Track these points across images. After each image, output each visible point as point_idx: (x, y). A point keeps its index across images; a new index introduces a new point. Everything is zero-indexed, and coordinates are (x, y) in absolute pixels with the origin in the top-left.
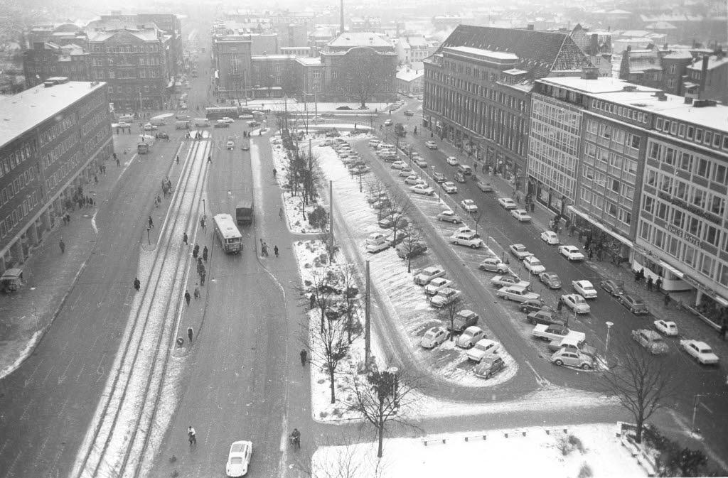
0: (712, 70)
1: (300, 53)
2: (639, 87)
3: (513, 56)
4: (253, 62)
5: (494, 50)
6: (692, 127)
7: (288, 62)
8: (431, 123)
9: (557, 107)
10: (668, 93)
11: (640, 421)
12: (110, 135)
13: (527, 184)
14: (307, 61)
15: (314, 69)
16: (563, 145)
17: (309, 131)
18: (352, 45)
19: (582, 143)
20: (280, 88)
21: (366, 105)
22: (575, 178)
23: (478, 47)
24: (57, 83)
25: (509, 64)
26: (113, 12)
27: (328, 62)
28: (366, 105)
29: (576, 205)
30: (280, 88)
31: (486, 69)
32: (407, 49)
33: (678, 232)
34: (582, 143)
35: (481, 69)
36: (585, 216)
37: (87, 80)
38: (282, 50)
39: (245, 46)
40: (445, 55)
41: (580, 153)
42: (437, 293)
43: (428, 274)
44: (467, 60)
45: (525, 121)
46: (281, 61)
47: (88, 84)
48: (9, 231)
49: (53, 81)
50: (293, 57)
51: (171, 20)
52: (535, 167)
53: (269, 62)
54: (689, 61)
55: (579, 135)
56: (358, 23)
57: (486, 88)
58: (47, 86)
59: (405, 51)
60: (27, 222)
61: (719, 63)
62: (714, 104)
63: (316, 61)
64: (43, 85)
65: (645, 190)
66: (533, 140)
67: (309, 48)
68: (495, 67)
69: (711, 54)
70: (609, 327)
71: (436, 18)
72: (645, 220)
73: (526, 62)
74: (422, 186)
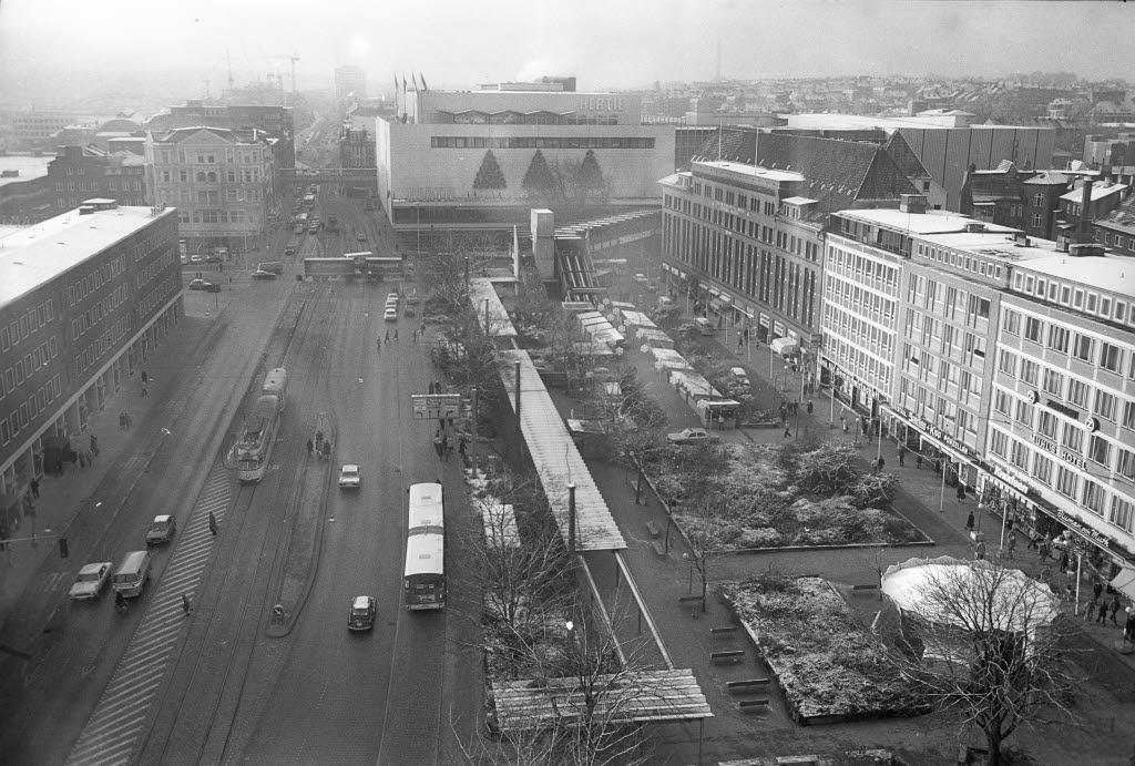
0: (1099, 201)
2: (990, 226)
5: (769, 168)
6: (1095, 294)
10: (139, 236)
12: (180, 288)
16: (870, 274)
22: (893, 362)
23: (745, 162)
24: (100, 207)
26: (190, 103)
31: (720, 185)
33: (1048, 446)
35: (713, 185)
37: (146, 205)
40: (696, 174)
44: (753, 188)
47: (148, 210)
49: (93, 204)
51: (278, 117)
54: (1063, 188)
55: (898, 297)
58: (83, 212)
60: (43, 422)
61: (1108, 191)
62: (1101, 253)
64: (78, 211)
65: (999, 382)
69: (1095, 178)
73: (817, 187)
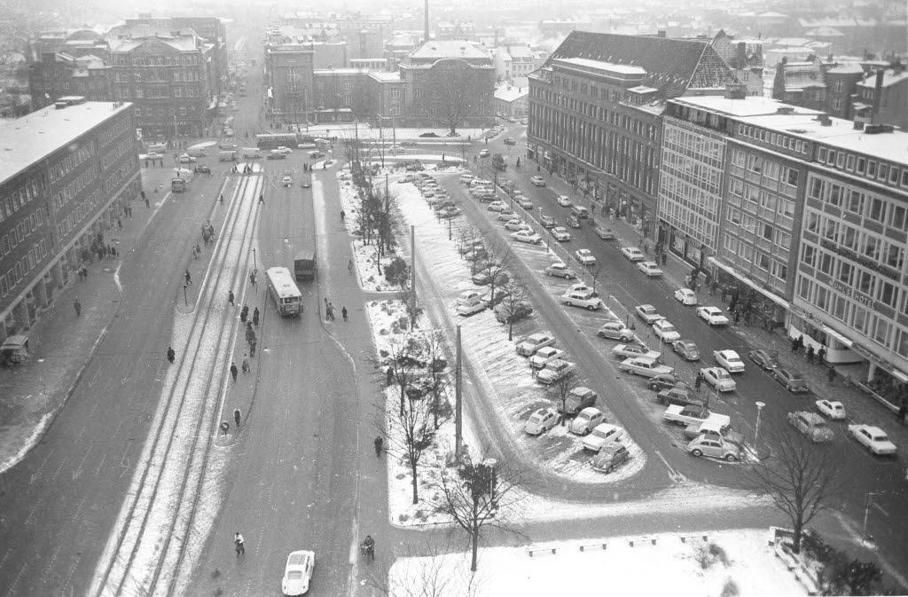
0: (889, 87)
1: (374, 66)
2: (798, 109)
3: (640, 71)
4: (316, 77)
5: (616, 63)
6: (863, 159)
7: (359, 77)
8: (537, 154)
9: (695, 134)
10: (833, 116)
11: (799, 526)
12: (138, 168)
13: (657, 230)
14: (382, 76)
15: (392, 86)
16: (702, 181)
17: (385, 163)
18: (439, 56)
19: (725, 179)
20: (349, 110)
21: (457, 131)
22: (718, 222)
23: (596, 59)
24: (71, 103)
25: (635, 80)
26: (141, 15)
27: (409, 78)
28: (457, 131)
29: (718, 256)
30: (349, 110)
31: (606, 86)
32: (507, 62)
33: (845, 290)
34: (725, 179)
35: (600, 86)
36: (730, 270)
37: (108, 100)
38: (352, 63)
39: (305, 57)
40: (555, 68)
41: (724, 192)
42: (544, 366)
43: (534, 342)
44: (582, 75)
45: (654, 151)
46: (350, 76)
47: (110, 104)
48: (11, 289)
49: (65, 101)
50: (365, 71)
51: (214, 25)
52: (667, 209)
53: (335, 77)
54: (859, 77)
55: (722, 169)
56: (447, 29)
57: (606, 111)
58: (58, 107)
59: (505, 64)
60: (33, 278)
61: (897, 79)
62: (890, 130)
63: (394, 77)
64: (54, 106)
65: (804, 237)
66: (665, 175)
67: (385, 60)
68: (618, 83)
69: (886, 68)
70: (759, 408)
71: (544, 22)
72: (805, 275)
73: (656, 78)
74: (526, 232)
